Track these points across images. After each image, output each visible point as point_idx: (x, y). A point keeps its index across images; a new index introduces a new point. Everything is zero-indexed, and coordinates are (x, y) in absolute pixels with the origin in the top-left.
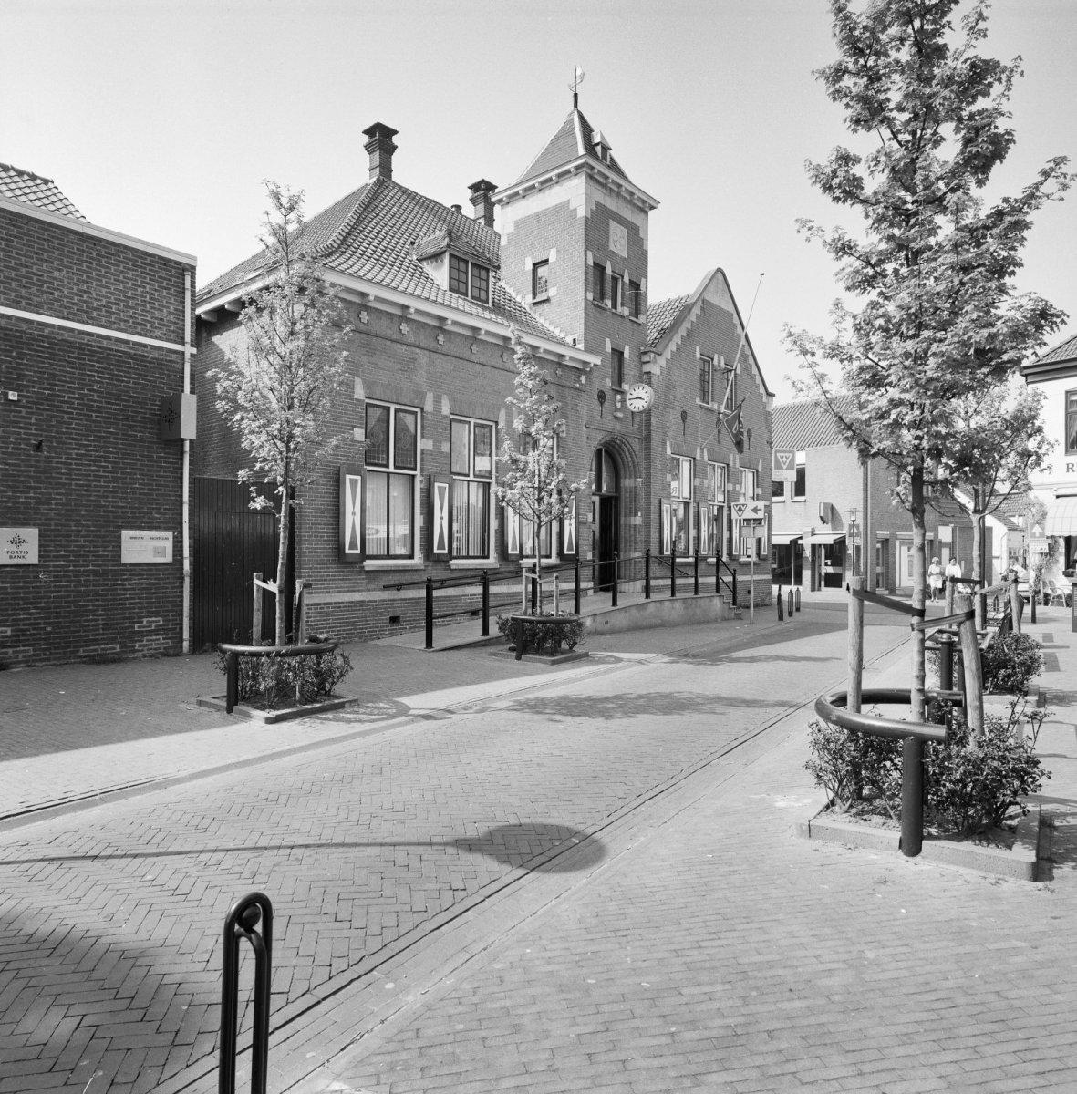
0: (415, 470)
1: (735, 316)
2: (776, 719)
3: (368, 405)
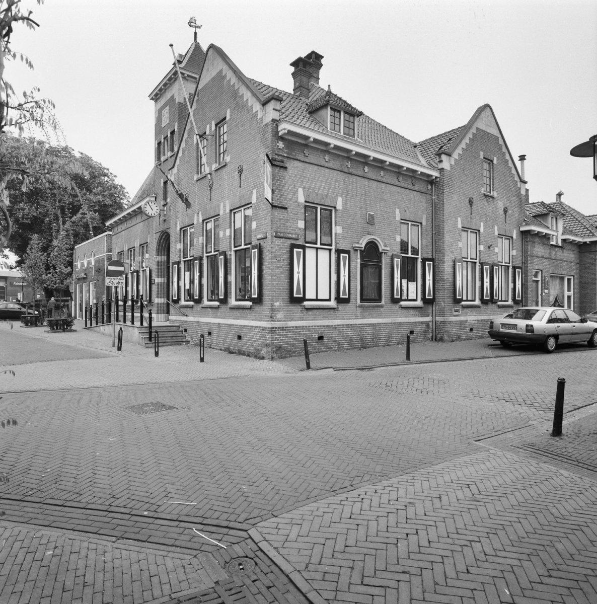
0: (418, 255)
1: (500, 139)
2: (482, 437)
3: (306, 206)
